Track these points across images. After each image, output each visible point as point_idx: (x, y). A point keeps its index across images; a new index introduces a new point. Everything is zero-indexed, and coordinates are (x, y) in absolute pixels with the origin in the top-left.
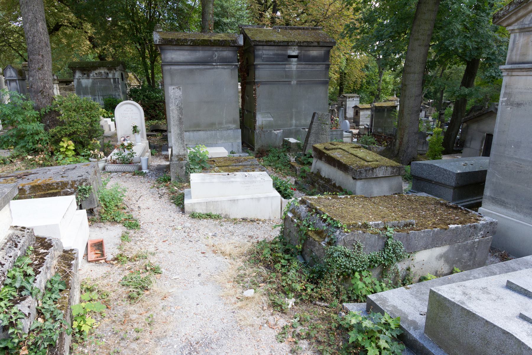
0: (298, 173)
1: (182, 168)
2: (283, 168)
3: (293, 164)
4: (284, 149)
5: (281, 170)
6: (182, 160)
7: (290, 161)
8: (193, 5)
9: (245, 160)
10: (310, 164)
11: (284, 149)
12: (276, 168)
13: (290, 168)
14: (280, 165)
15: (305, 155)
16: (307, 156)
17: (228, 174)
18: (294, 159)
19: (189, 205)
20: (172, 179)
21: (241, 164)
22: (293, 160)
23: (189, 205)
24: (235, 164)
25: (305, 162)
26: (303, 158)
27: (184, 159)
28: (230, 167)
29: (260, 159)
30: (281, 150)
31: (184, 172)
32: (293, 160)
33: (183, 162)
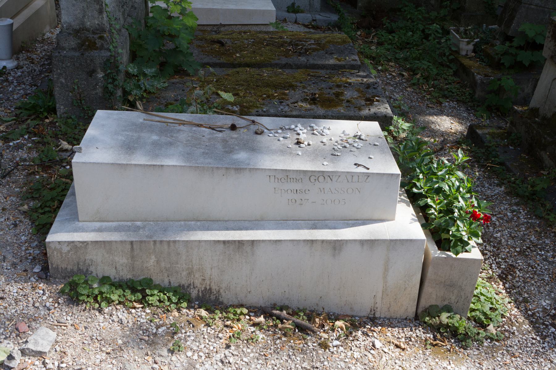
0: (479, 93)
1: (91, 73)
2: (435, 71)
3: (466, 62)
4: (443, 12)
5: (427, 79)
6: (92, 46)
7: (457, 52)
8: (461, 156)
9: (320, 46)
10: (493, 45)
11: (443, 12)
12: (413, 71)
13: (455, 74)
14: (425, 64)
15: (508, 39)
16: (516, 43)
17: (233, 127)
18: (471, 47)
19: (65, 249)
20: (61, 109)
21: (303, 59)
22: (466, 47)
23: (65, 249)
24: (284, 61)
25: (506, 61)
26: (499, 47)
27: (99, 43)
28: (266, 73)
29: (368, 35)
30: (434, 14)
31: (99, 91)
32: (466, 47)
33: (95, 53)
